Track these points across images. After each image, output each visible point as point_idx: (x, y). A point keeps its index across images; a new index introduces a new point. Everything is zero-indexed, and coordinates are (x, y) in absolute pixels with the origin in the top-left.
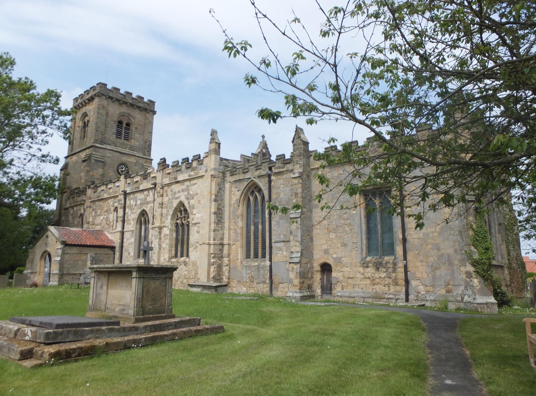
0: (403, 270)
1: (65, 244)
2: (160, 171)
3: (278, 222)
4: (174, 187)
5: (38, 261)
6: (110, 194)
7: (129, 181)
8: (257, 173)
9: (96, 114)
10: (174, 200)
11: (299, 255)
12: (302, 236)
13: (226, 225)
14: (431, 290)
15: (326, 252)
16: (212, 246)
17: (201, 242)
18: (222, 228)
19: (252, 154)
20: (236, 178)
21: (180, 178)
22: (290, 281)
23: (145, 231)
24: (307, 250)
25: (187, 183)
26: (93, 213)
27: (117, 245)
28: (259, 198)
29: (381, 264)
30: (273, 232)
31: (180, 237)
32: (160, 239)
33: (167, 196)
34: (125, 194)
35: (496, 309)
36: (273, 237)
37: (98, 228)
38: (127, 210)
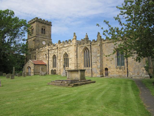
0: (127, 69)
1: (35, 64)
2: (59, 44)
3: (93, 58)
4: (63, 48)
5: (26, 69)
7: (49, 47)
8: (87, 45)
9: (36, 27)
11: (100, 66)
12: (100, 61)
13: (79, 58)
15: (106, 65)
16: (75, 64)
17: (72, 63)
18: (78, 59)
19: (84, 39)
20: (81, 46)
21: (65, 46)
22: (98, 73)
23: (55, 60)
24: (102, 65)
25: (67, 47)
26: (39, 55)
27: (47, 64)
28: (88, 51)
29: (121, 68)
30: (92, 60)
31: (66, 62)
32: (60, 62)
33: (61, 51)
34: (48, 50)
35: (149, 78)
36: (92, 61)
37: (41, 60)
38: (49, 55)
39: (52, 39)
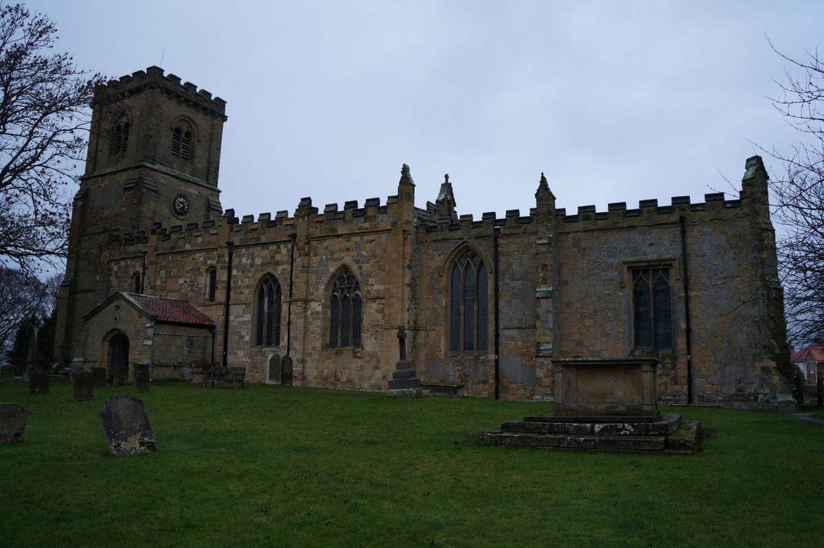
0: (685, 366)
2: (303, 217)
4: (327, 243)
6: (197, 245)
10: (330, 262)
14: (719, 389)
15: (579, 343)
25: (357, 239)
30: (501, 316)
33: (316, 255)
38: (234, 272)
39: (219, 187)
